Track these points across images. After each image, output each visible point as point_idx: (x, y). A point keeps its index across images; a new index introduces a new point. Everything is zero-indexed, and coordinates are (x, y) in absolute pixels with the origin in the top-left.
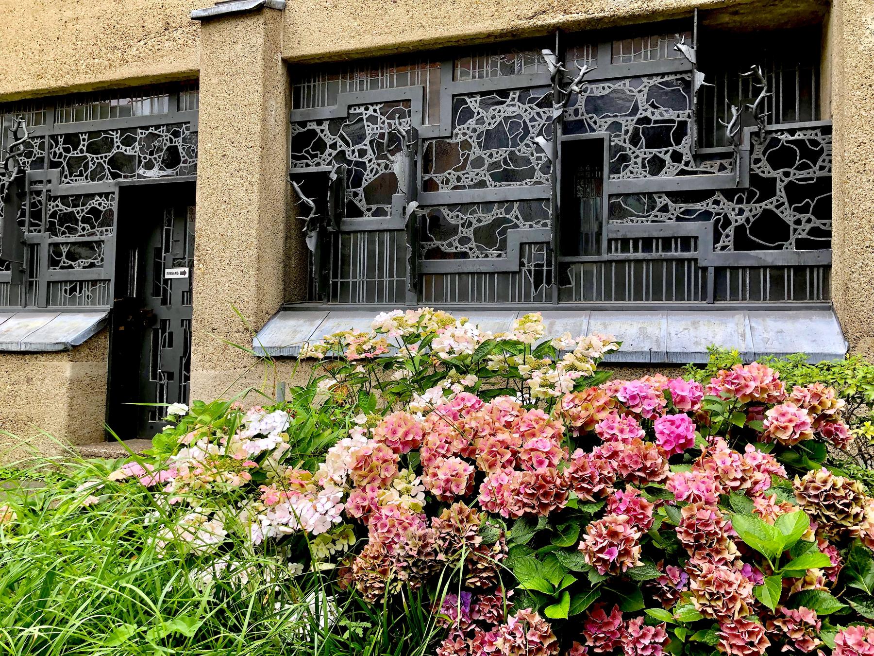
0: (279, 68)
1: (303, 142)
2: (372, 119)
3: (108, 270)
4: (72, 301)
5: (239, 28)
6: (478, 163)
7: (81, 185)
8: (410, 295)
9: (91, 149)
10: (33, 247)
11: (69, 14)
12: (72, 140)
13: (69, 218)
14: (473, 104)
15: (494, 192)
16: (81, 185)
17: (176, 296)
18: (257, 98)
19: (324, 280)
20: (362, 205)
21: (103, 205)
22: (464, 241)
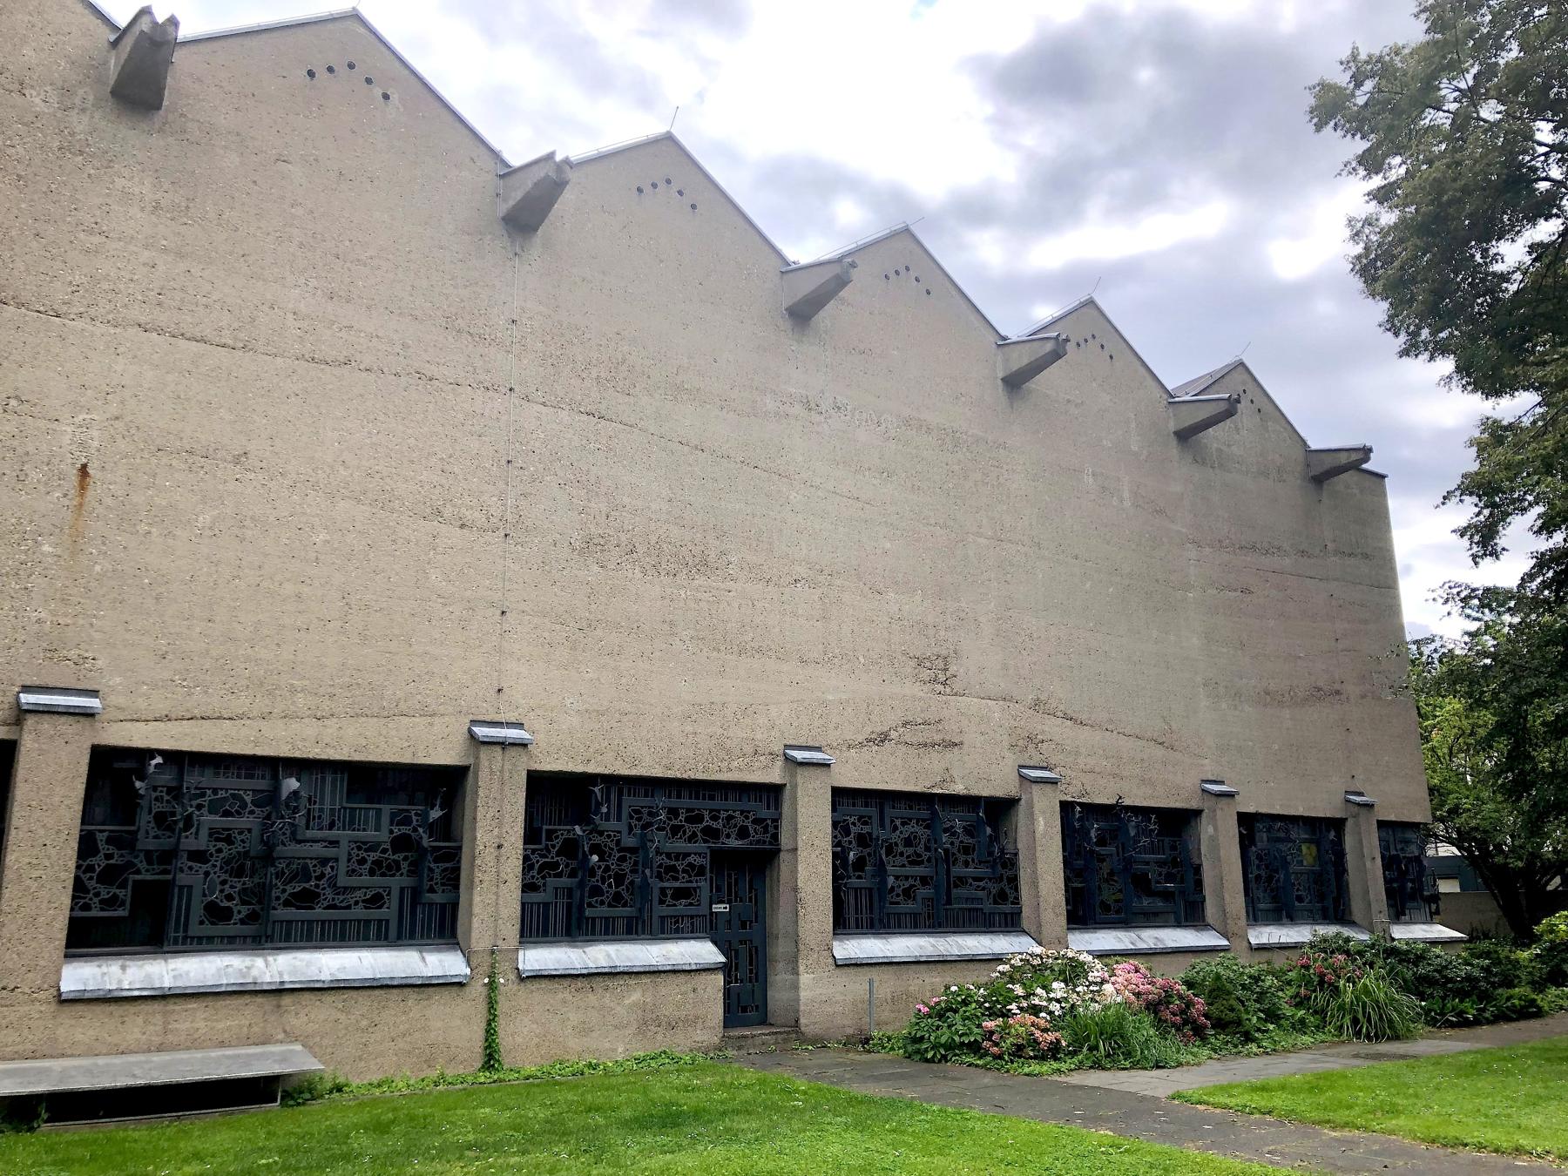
6: (902, 854)
7: (680, 845)
13: (673, 869)
15: (910, 870)
16: (680, 845)
21: (698, 861)
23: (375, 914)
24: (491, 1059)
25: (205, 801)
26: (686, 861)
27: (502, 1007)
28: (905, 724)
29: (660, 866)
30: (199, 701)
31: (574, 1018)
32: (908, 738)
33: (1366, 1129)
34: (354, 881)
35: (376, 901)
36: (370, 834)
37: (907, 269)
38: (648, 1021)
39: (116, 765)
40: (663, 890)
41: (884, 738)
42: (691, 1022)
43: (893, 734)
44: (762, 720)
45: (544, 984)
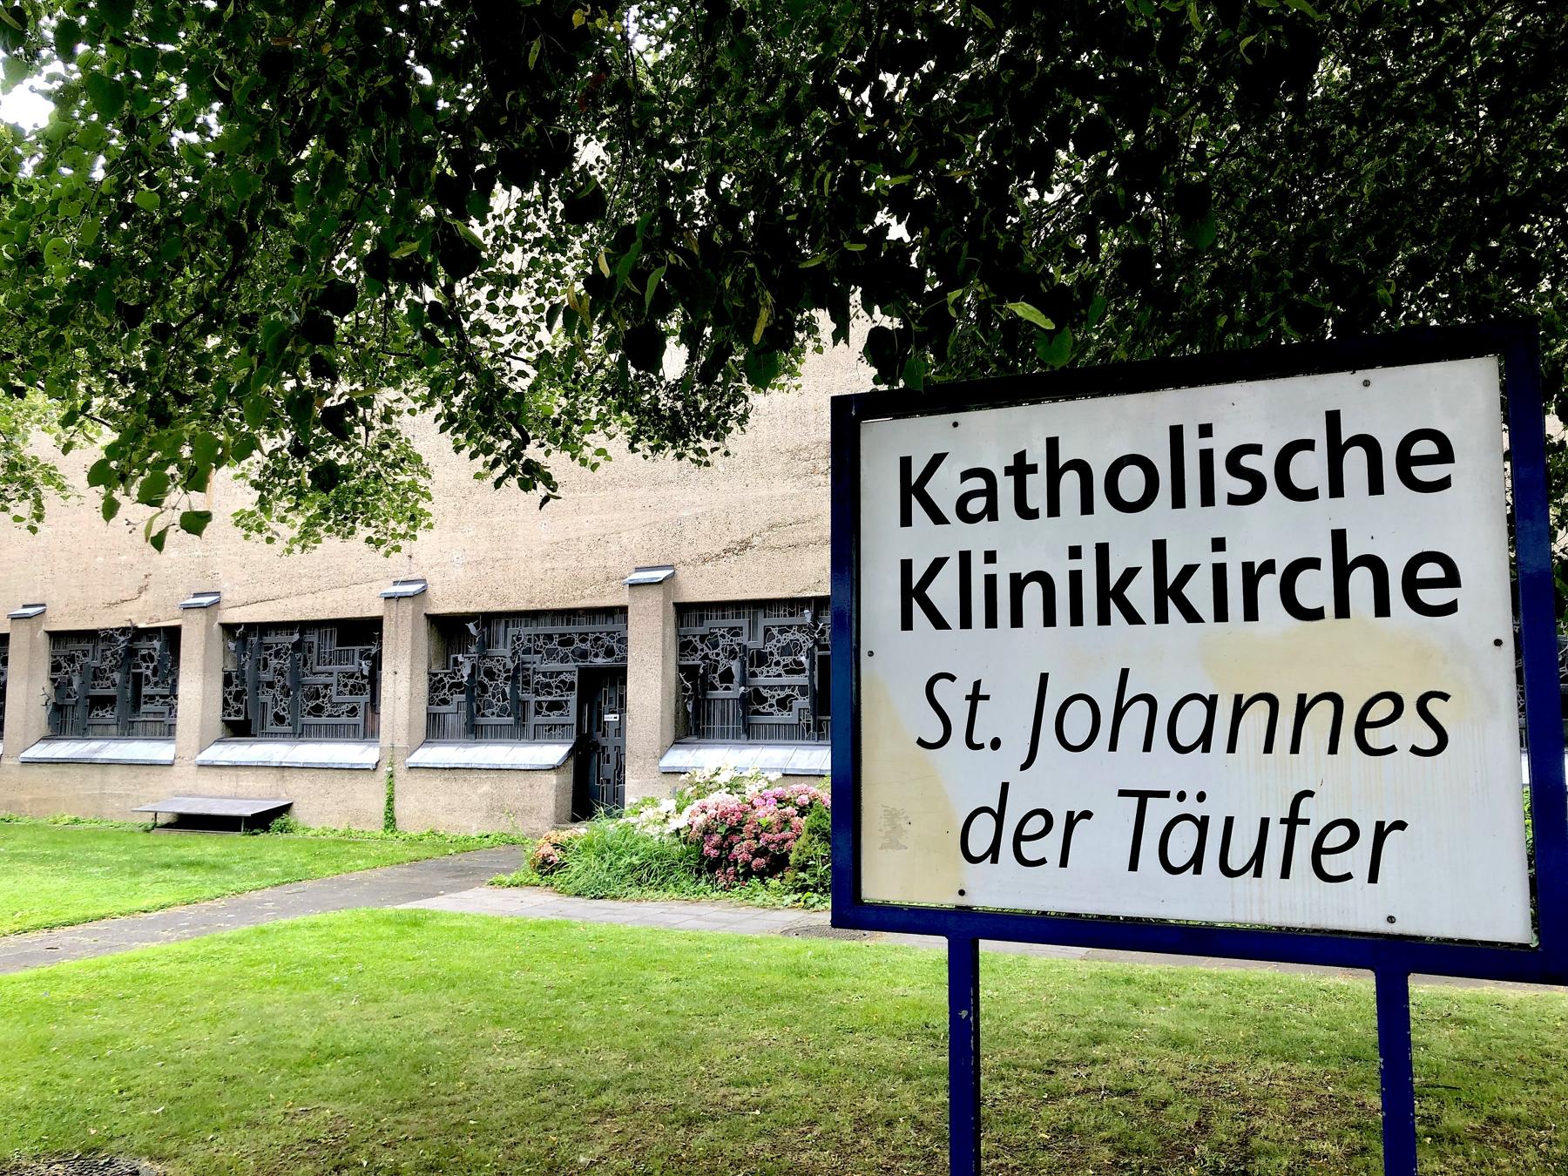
0: (672, 608)
1: (685, 647)
2: (723, 636)
3: (572, 718)
4: (550, 737)
5: (649, 591)
6: (777, 664)
7: (555, 666)
8: (744, 736)
9: (561, 643)
10: (525, 703)
11: (548, 565)
12: (549, 637)
13: (548, 685)
14: (775, 631)
15: (787, 680)
16: (555, 666)
17: (611, 731)
18: (660, 629)
19: (697, 726)
20: (717, 684)
21: (568, 678)
22: (771, 706)
23: (353, 720)
24: (391, 821)
25: (272, 651)
27: (398, 787)
28: (771, 527)
30: (265, 591)
31: (443, 800)
32: (774, 542)
33: (131, 913)
34: (341, 699)
35: (353, 711)
36: (350, 668)
38: (495, 808)
40: (539, 704)
41: (745, 545)
42: (528, 812)
43: (756, 541)
44: (614, 548)
45: (424, 773)
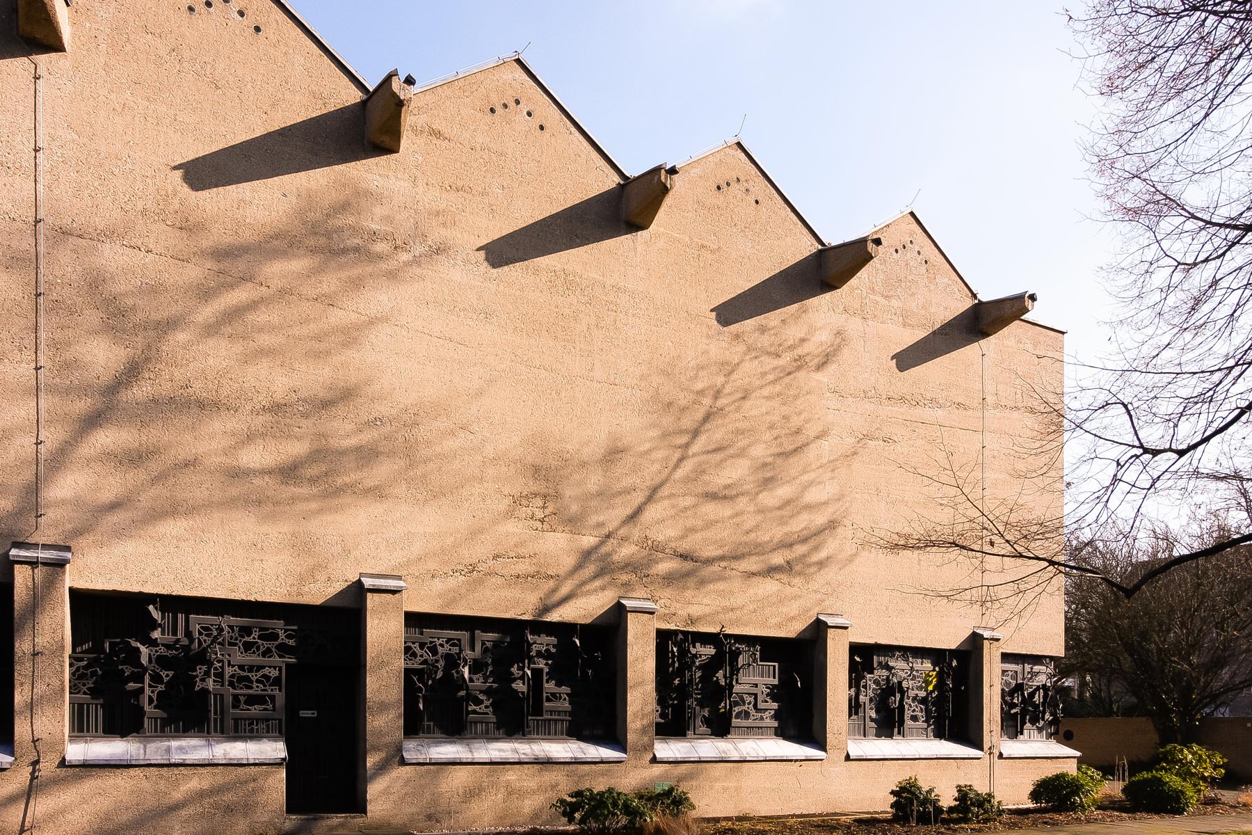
13: (247, 679)
26: (260, 674)
28: (496, 557)
29: (232, 676)
37: (517, 102)
39: (151, 608)
40: (236, 697)
